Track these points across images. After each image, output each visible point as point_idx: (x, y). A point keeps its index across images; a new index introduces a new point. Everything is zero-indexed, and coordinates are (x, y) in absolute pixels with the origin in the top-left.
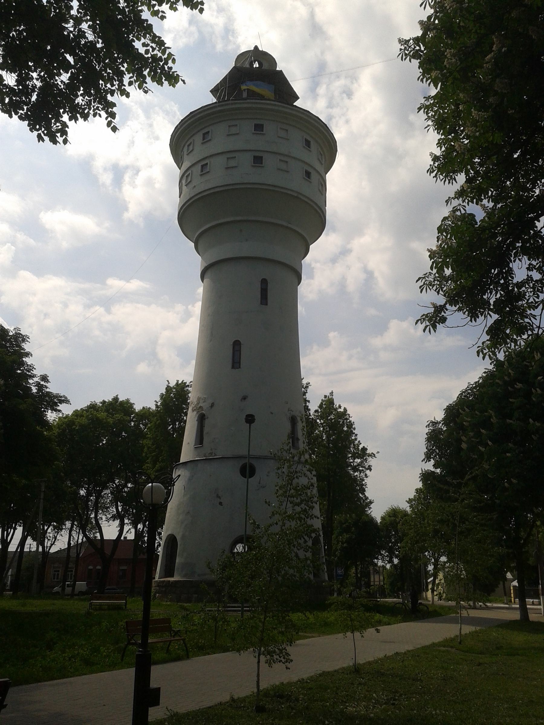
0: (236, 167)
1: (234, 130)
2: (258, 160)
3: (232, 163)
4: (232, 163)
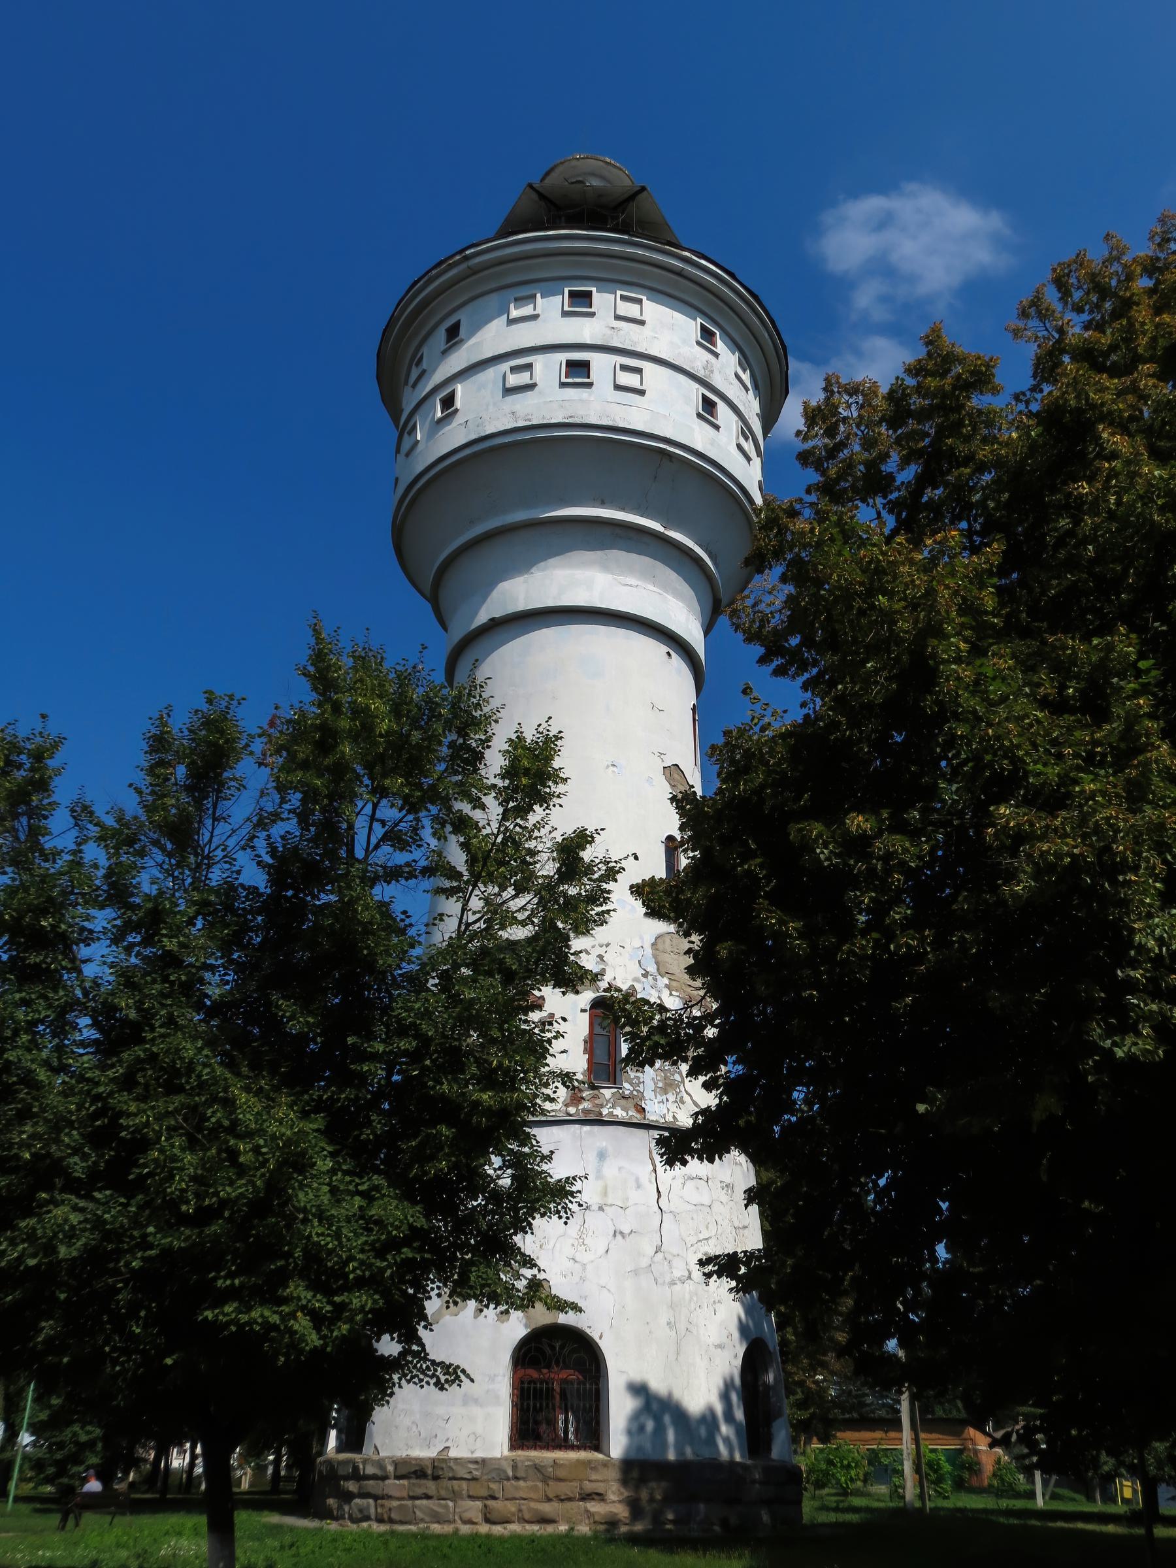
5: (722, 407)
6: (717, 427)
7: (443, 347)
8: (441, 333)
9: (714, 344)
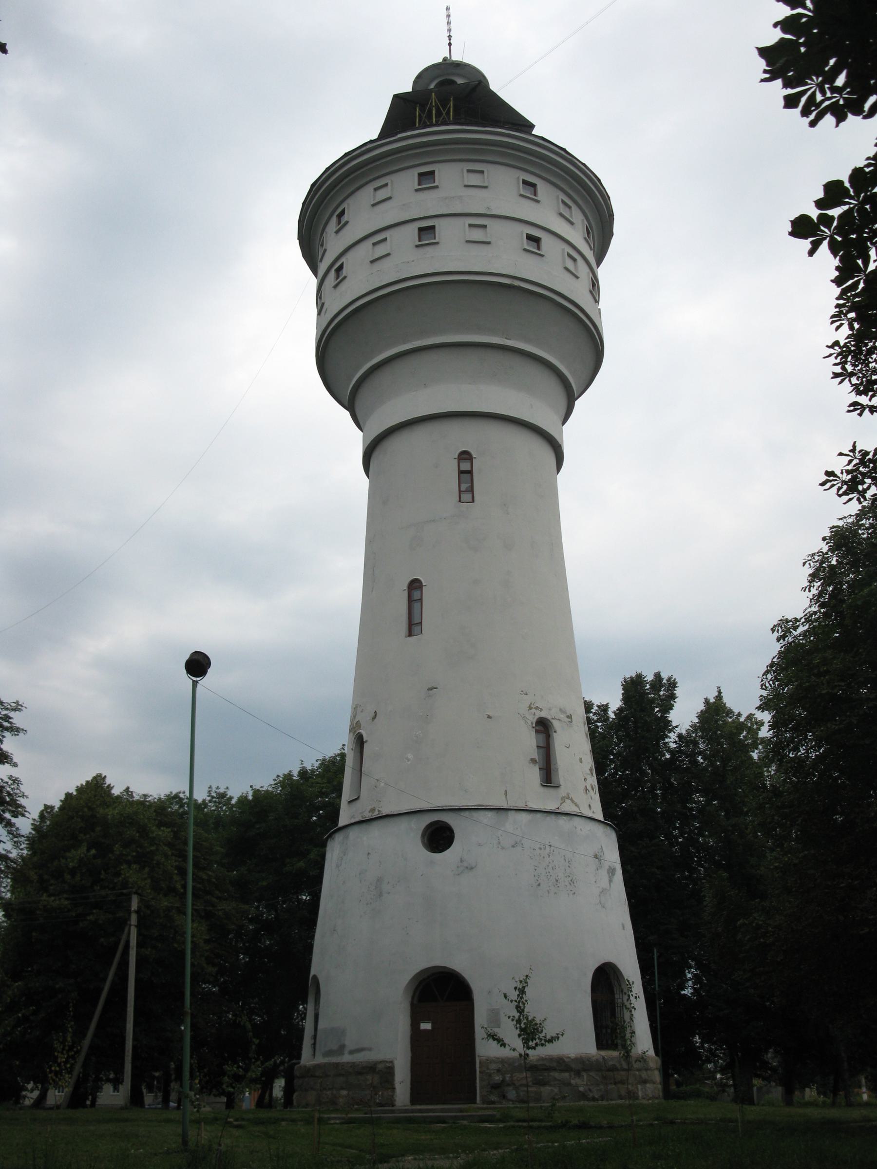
0: (388, 255)
1: (382, 194)
2: (427, 232)
3: (381, 250)
4: (381, 250)
5: (547, 241)
6: (542, 256)
7: (335, 230)
8: (334, 219)
9: (535, 195)
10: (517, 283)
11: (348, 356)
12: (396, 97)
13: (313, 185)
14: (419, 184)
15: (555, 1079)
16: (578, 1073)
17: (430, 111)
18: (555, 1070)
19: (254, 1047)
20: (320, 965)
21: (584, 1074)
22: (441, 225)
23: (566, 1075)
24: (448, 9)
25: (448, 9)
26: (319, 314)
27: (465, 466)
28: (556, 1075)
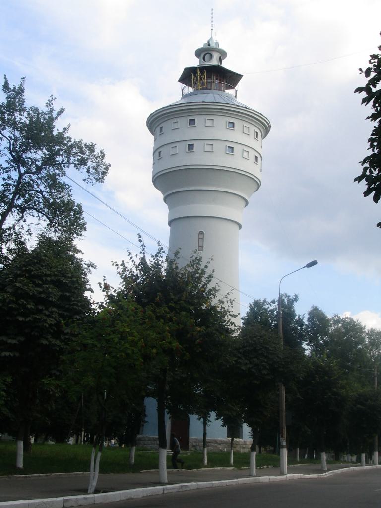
1: (175, 126)
5: (237, 148)
10: (222, 168)
11: (161, 179)
12: (186, 69)
13: (151, 114)
14: (190, 125)
15: (212, 445)
16: (220, 444)
17: (197, 78)
18: (212, 442)
19: (285, 444)
20: (149, 398)
21: (222, 445)
22: (196, 144)
23: (216, 444)
24: (212, 10)
25: (212, 10)
26: (155, 141)
27: (201, 236)
28: (213, 444)
